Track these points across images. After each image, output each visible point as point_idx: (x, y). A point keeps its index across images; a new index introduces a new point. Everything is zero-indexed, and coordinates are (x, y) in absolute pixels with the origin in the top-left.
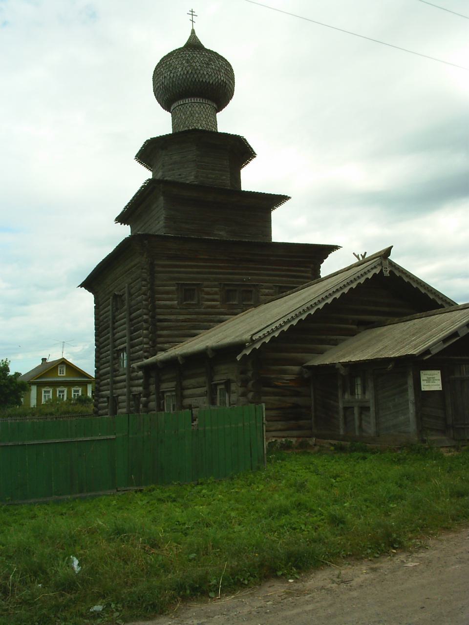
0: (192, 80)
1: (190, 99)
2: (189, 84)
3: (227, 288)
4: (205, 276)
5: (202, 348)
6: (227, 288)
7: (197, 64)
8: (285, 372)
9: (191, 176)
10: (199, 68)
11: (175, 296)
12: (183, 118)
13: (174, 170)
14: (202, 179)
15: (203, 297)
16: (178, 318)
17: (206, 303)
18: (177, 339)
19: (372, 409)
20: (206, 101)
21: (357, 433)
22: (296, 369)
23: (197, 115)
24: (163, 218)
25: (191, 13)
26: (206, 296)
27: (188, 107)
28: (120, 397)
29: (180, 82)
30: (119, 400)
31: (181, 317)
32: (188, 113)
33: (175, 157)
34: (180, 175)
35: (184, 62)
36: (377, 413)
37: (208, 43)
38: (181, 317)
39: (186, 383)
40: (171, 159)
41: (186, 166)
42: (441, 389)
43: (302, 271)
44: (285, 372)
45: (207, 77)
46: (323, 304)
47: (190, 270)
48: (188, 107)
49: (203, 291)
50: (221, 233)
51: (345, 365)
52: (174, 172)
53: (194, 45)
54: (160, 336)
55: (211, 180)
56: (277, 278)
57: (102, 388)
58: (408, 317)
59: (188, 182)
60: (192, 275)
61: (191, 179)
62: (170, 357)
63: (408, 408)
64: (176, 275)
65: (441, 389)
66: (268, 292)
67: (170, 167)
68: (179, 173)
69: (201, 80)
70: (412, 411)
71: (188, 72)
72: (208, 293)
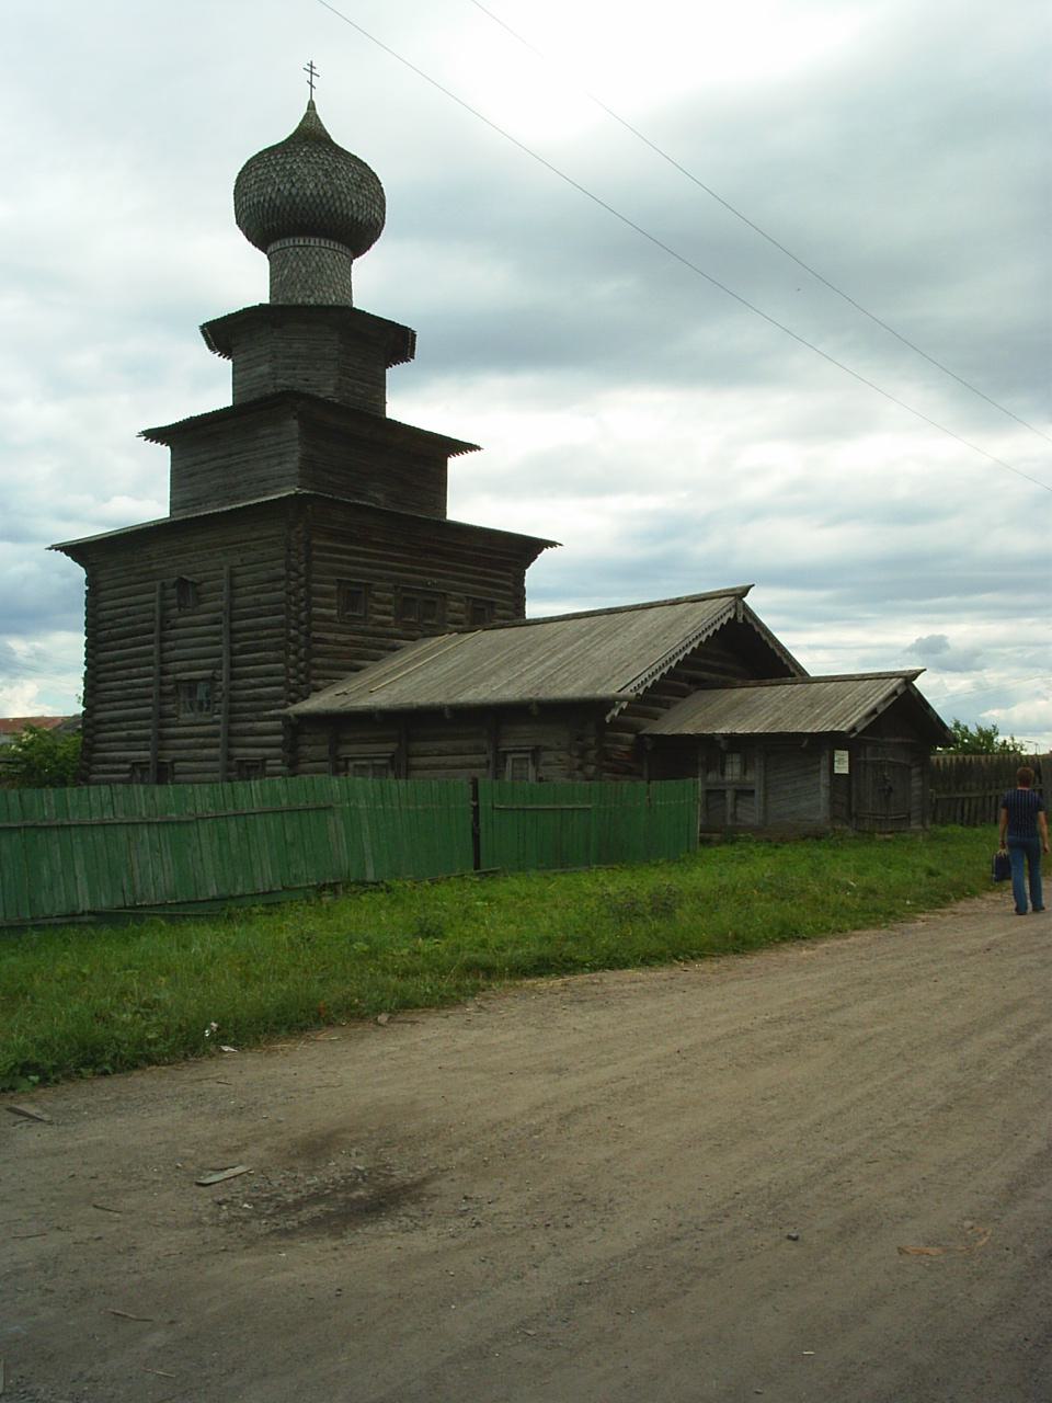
0: (330, 210)
1: (317, 240)
2: (323, 214)
3: (404, 595)
5: (477, 702)
6: (404, 595)
7: (342, 182)
8: (618, 741)
10: (345, 190)
11: (335, 601)
12: (304, 271)
13: (294, 369)
14: (346, 394)
15: (372, 607)
16: (339, 639)
17: (376, 616)
18: (342, 674)
19: (759, 793)
21: (729, 823)
22: (631, 736)
23: (328, 272)
24: (295, 459)
25: (309, 68)
26: (376, 606)
27: (313, 253)
28: (176, 765)
29: (307, 207)
30: (177, 769)
31: (342, 638)
32: (314, 264)
35: (320, 173)
36: (766, 796)
37: (342, 135)
38: (342, 638)
39: (417, 746)
40: (290, 348)
42: (847, 772)
43: (501, 577)
44: (618, 741)
45: (355, 208)
46: (683, 654)
47: (327, 555)
48: (313, 253)
49: (373, 596)
50: (377, 496)
51: (725, 736)
53: (311, 135)
54: (315, 666)
58: (774, 681)
59: (322, 396)
60: (359, 569)
61: (327, 391)
62: (415, 706)
63: (819, 791)
64: (338, 566)
65: (847, 772)
67: (288, 361)
68: (306, 377)
69: (345, 212)
70: (823, 796)
71: (325, 194)
72: (379, 601)
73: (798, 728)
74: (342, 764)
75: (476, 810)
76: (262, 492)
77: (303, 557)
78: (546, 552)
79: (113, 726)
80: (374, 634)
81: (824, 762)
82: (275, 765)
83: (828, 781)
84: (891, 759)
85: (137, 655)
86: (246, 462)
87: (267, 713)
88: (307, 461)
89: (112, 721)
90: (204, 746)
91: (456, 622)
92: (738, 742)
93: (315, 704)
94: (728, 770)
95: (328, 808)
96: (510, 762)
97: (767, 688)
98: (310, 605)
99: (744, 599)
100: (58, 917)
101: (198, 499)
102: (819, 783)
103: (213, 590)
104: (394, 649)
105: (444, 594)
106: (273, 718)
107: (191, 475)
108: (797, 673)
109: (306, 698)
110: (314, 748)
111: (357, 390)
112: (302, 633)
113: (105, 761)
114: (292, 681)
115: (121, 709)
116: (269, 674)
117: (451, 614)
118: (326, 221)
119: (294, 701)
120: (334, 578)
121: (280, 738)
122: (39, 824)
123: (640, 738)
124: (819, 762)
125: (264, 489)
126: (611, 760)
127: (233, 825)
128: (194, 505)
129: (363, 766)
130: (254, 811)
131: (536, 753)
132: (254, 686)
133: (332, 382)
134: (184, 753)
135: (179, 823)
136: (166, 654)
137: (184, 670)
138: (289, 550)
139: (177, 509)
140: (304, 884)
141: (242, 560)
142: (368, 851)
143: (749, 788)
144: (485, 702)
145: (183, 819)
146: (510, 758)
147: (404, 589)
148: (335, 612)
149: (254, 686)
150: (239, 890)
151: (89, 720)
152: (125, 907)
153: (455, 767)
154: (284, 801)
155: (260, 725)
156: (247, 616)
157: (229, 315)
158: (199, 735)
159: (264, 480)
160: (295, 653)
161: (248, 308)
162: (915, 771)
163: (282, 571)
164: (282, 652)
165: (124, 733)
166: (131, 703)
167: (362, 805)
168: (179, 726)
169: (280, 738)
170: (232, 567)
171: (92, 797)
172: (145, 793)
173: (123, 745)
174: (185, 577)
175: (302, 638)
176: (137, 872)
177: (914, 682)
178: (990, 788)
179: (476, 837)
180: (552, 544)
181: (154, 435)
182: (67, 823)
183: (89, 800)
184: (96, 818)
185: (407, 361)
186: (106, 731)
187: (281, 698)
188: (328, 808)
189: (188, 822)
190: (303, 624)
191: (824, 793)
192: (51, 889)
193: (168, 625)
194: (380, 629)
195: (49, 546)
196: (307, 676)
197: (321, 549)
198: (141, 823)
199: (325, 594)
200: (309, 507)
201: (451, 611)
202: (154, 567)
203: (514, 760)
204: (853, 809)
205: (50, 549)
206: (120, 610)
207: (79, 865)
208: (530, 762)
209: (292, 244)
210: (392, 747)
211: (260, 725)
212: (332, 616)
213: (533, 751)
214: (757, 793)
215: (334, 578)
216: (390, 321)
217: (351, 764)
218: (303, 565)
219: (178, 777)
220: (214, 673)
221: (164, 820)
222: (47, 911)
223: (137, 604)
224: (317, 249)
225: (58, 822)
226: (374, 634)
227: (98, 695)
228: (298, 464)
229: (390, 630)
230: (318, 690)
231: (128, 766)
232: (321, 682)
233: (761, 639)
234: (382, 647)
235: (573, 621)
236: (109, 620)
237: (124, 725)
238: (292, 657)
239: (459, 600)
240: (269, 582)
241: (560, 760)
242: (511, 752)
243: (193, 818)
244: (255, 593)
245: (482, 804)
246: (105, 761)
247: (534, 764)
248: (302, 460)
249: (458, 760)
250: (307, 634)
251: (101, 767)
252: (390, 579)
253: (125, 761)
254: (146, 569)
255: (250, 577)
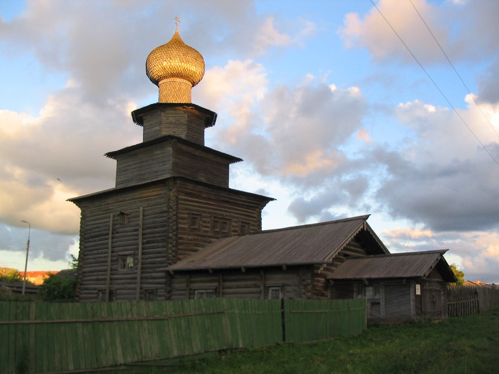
4: (204, 210)
8: (318, 281)
9: (183, 134)
16: (188, 238)
20: (188, 82)
24: (171, 163)
31: (190, 237)
33: (171, 119)
34: (174, 132)
40: (168, 120)
41: (179, 127)
42: (420, 294)
52: (170, 129)
54: (179, 249)
55: (194, 140)
56: (240, 216)
57: (84, 282)
61: (183, 137)
64: (188, 207)
65: (420, 294)
66: (405, 243)
67: (167, 125)
68: (174, 131)
72: (204, 222)
73: (399, 275)
74: (192, 292)
75: (283, 314)
76: (156, 177)
77: (175, 203)
78: (270, 203)
79: (90, 274)
80: (203, 236)
81: (412, 290)
82: (161, 292)
83: (414, 297)
84: (435, 288)
85: (101, 244)
86: (149, 165)
87: (158, 269)
88: (175, 164)
89: (90, 272)
90: (130, 283)
91: (236, 231)
92: (372, 282)
93: (179, 266)
94: (367, 293)
95: (223, 312)
96: (270, 291)
97: (379, 258)
98: (177, 223)
99: (366, 220)
100: (109, 367)
101: (127, 180)
102: (410, 299)
103: (134, 217)
104: (210, 242)
105: (230, 219)
106: (161, 271)
107: (125, 171)
108: (386, 252)
109: (175, 263)
110: (180, 284)
111: (194, 136)
112: (174, 235)
113: (86, 289)
114: (170, 256)
115: (94, 267)
116: (159, 253)
117: (233, 228)
118: (183, 72)
119: (170, 264)
120: (187, 212)
121: (164, 280)
122: (100, 320)
123: (328, 281)
124: (410, 290)
125: (156, 176)
126: (316, 290)
127: (183, 321)
128: (126, 183)
129: (202, 293)
130: (191, 314)
131: (283, 286)
132: (152, 258)
133: (184, 133)
134: (120, 286)
135: (160, 320)
136: (114, 244)
137: (121, 251)
138: (169, 200)
139: (118, 185)
140: (213, 350)
141: (148, 204)
142: (239, 333)
143: (377, 301)
144: (199, 268)
145: (162, 318)
146: (270, 289)
147: (215, 217)
148: (187, 226)
149: (152, 258)
150: (187, 353)
151: (80, 272)
152: (139, 362)
153: (245, 293)
154: (204, 310)
155: (155, 275)
156: (150, 228)
157: (150, 105)
158: (128, 279)
159: (156, 172)
160: (171, 243)
161: (152, 104)
162: (442, 293)
163: (165, 209)
164: (165, 243)
165: (94, 278)
166: (98, 264)
167: (236, 311)
168: (119, 274)
169: (164, 280)
170: (144, 207)
171: (122, 307)
172: (145, 305)
173: (94, 282)
174: (123, 212)
175: (174, 237)
176: (143, 344)
177: (443, 255)
178: (459, 300)
179: (284, 326)
180: (272, 199)
181: (111, 155)
182: (112, 320)
183: (121, 308)
184: (125, 317)
185: (212, 126)
186: (87, 276)
187: (165, 263)
188: (223, 312)
189: (164, 319)
190: (174, 231)
191: (412, 303)
192: (106, 353)
193: (115, 232)
194: (204, 234)
195: (67, 199)
196: (176, 253)
197: (182, 200)
198: (144, 320)
199: (183, 219)
200: (179, 182)
201: (233, 227)
202: (110, 208)
203: (273, 290)
204: (423, 310)
205: (67, 200)
206: (94, 226)
207: (118, 341)
208: (280, 291)
209: (169, 81)
210: (215, 284)
211: (155, 275)
212: (186, 228)
213: (282, 286)
214: (381, 304)
215: (187, 212)
216: (208, 110)
217: (196, 292)
218: (175, 206)
219: (118, 296)
220: (135, 252)
221: (154, 318)
222: (104, 364)
223: (102, 223)
224: (179, 83)
225: (109, 319)
226: (203, 236)
227: (178, 256)
228: (171, 165)
229: (208, 234)
230: (180, 259)
231: (96, 291)
232: (181, 256)
233: (373, 237)
234: (206, 242)
235: (290, 231)
236: (90, 230)
237: (95, 274)
238: (170, 245)
239: (236, 222)
240: (159, 213)
241: (294, 290)
242: (271, 287)
243: (166, 318)
244: (153, 218)
245: (286, 311)
246: (86, 289)
247: (282, 291)
248: (173, 164)
249: (246, 290)
250: (176, 235)
251: (85, 291)
252: (209, 213)
253: (95, 289)
254: (106, 209)
255: (150, 212)
